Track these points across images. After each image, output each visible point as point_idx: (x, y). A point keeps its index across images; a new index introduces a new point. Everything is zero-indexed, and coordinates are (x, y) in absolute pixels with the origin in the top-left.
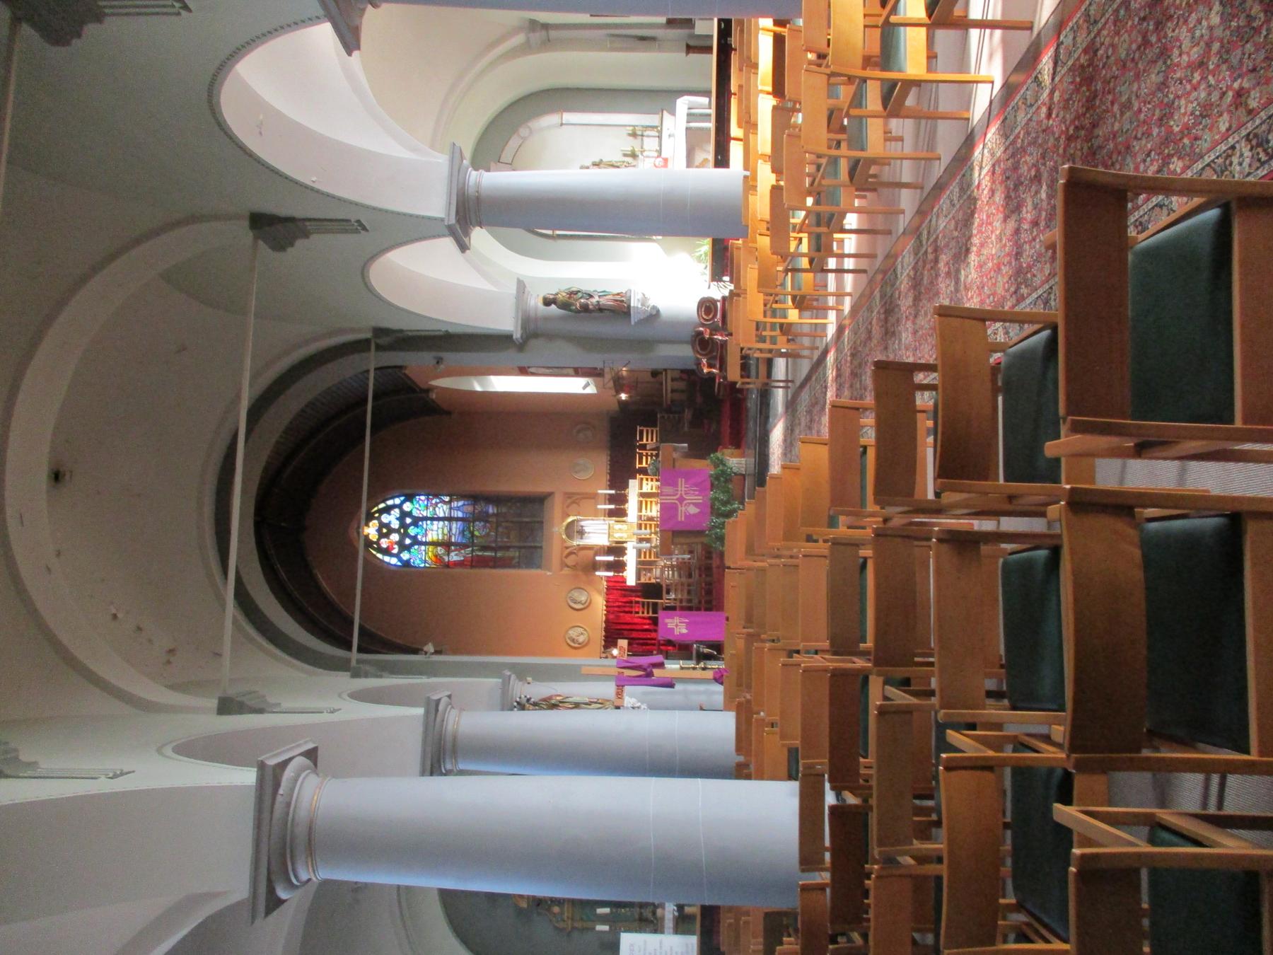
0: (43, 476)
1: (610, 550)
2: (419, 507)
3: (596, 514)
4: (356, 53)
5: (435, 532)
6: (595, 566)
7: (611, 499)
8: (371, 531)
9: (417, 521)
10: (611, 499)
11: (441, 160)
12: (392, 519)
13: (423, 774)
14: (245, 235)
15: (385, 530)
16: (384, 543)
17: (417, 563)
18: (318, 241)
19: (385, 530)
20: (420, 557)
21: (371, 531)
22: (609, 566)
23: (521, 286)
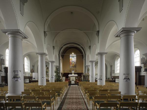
0: (143, 19)
1: (72, 73)
2: (75, 57)
3: (74, 72)
4: (27, 2)
5: (73, 59)
6: (70, 72)
7: (76, 73)
8: (73, 54)
9: (74, 57)
10: (76, 73)
11: (95, 60)
12: (74, 55)
13: (24, 77)
14: (90, 45)
15: (73, 55)
16: (72, 55)
17: (70, 58)
18: (89, 51)
19: (73, 55)
20: (71, 58)
21: (73, 54)
22: (70, 73)
23: (90, 66)
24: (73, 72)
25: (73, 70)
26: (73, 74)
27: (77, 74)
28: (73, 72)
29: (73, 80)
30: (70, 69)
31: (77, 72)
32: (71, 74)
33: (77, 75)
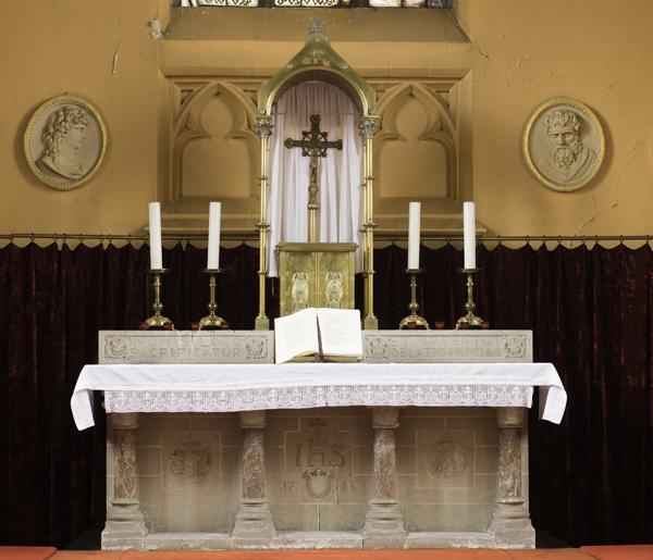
1: (242, 256)
6: (180, 200)
7: (441, 255)
10: (441, 255)
22: (186, 255)
24: (315, 200)
25: (319, 94)
26: (294, 331)
27: (495, 318)
28: (315, 200)
29: (335, 251)
30: (189, 80)
31: (519, 226)
32: (234, 293)
33: (503, 372)
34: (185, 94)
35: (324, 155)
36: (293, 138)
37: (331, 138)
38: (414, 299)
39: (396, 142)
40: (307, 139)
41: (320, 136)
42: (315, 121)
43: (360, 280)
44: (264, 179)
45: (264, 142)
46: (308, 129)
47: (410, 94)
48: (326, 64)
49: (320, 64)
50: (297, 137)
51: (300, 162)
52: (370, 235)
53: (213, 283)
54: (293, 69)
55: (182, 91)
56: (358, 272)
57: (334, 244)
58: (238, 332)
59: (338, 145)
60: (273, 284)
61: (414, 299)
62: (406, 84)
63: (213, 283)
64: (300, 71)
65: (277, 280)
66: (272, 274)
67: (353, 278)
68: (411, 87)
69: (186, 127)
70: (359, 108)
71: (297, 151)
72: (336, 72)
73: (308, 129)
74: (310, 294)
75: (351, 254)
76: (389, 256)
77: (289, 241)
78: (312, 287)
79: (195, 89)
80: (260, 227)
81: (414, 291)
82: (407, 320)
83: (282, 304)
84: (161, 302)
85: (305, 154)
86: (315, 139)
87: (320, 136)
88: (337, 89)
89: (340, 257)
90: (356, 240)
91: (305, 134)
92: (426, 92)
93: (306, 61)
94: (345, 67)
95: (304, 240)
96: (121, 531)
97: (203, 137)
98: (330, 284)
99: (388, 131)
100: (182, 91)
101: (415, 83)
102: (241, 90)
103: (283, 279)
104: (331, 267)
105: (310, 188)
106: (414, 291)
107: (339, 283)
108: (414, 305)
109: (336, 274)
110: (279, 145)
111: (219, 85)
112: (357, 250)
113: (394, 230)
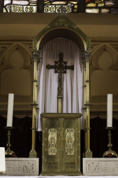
1: (24, 120)
25: (62, 42)
29: (70, 119)
34: (3, 49)
35: (65, 72)
36: (50, 65)
37: (69, 64)
38: (110, 142)
39: (98, 71)
40: (57, 65)
41: (63, 63)
42: (61, 56)
43: (83, 133)
44: (35, 81)
45: (35, 64)
46: (58, 60)
47: (104, 49)
48: (66, 26)
49: (63, 26)
50: (52, 63)
51: (54, 76)
52: (88, 110)
53: (9, 133)
54: (49, 29)
55: (1, 47)
56: (82, 129)
57: (70, 114)
58: (20, 159)
59: (72, 68)
60: (39, 135)
61: (110, 142)
62: (102, 44)
63: (9, 133)
64: (53, 29)
65: (41, 132)
66: (39, 130)
67: (79, 132)
68: (105, 45)
69: (3, 63)
70: (81, 46)
71: (52, 71)
72: (70, 29)
73: (58, 60)
74: (57, 138)
75: (79, 119)
76: (98, 121)
77: (48, 112)
78: (58, 136)
79: (7, 46)
80: (32, 105)
81: (110, 138)
82: (107, 153)
83: (43, 144)
84: (10, 143)
85: (56, 72)
86: (61, 65)
87: (63, 63)
88: (72, 41)
89: (73, 121)
90: (80, 112)
91: (56, 62)
92: (112, 48)
93: (56, 24)
94: (75, 27)
95: (55, 111)
96: (98, 114)
97: (11, 68)
98: (68, 135)
99: (95, 65)
100: (1, 47)
101: (107, 44)
102: (28, 47)
103: (44, 132)
104: (68, 126)
105: (58, 88)
106: (110, 138)
107: (72, 134)
108: (110, 145)
109: (71, 129)
110: (43, 68)
111: (18, 45)
112: (81, 118)
113: (98, 110)
